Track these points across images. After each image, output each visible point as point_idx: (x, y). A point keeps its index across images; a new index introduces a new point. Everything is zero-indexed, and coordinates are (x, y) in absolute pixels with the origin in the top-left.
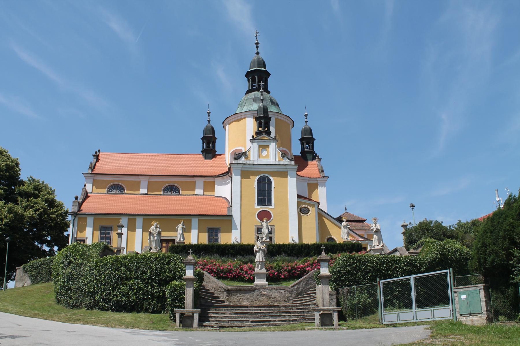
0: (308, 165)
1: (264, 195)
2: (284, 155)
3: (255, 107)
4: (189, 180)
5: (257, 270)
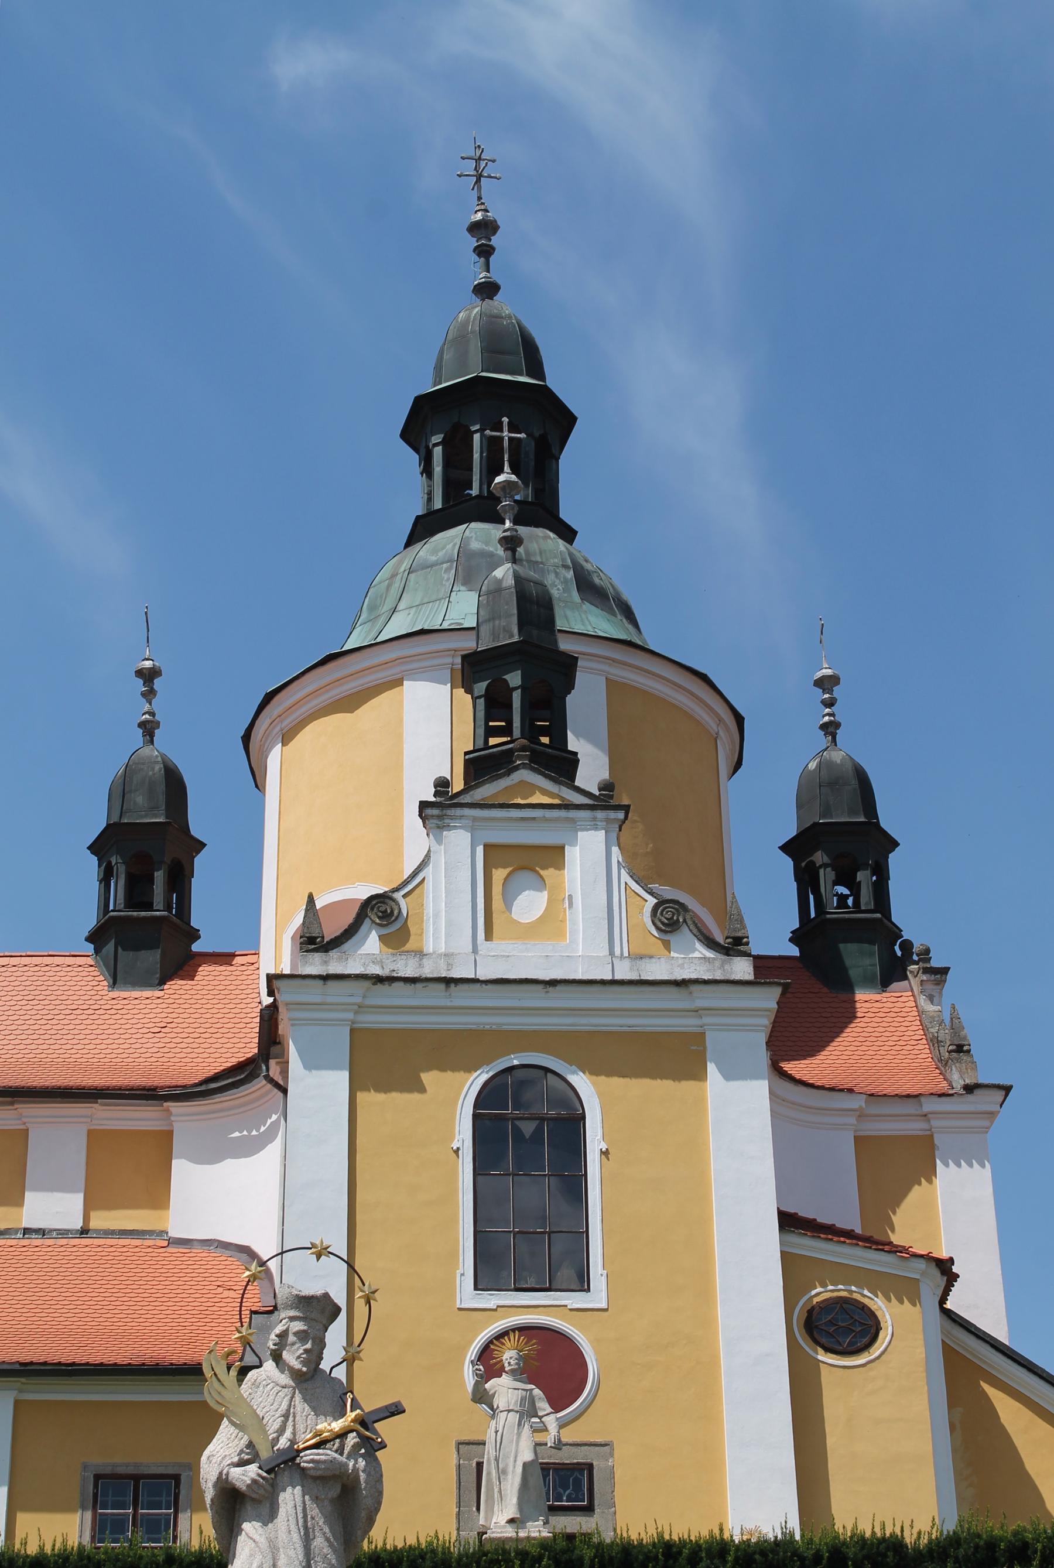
0: (850, 1016)
1: (529, 1146)
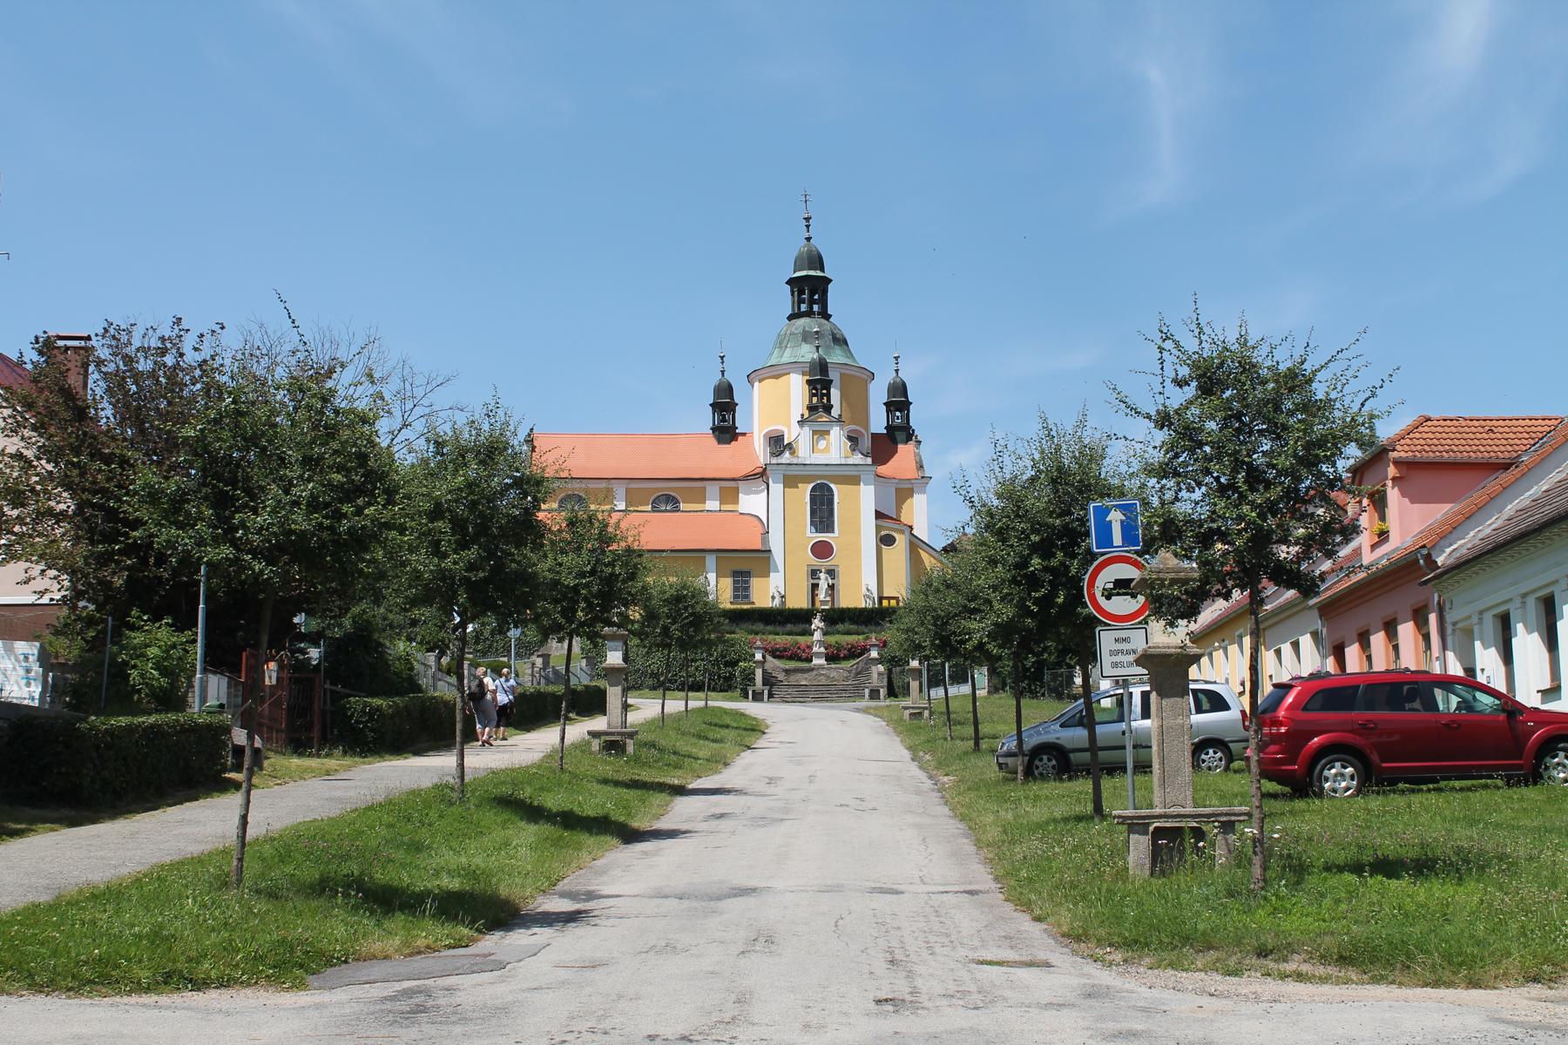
1: (822, 511)
2: (853, 439)
3: (807, 353)
4: (695, 486)
5: (815, 649)
